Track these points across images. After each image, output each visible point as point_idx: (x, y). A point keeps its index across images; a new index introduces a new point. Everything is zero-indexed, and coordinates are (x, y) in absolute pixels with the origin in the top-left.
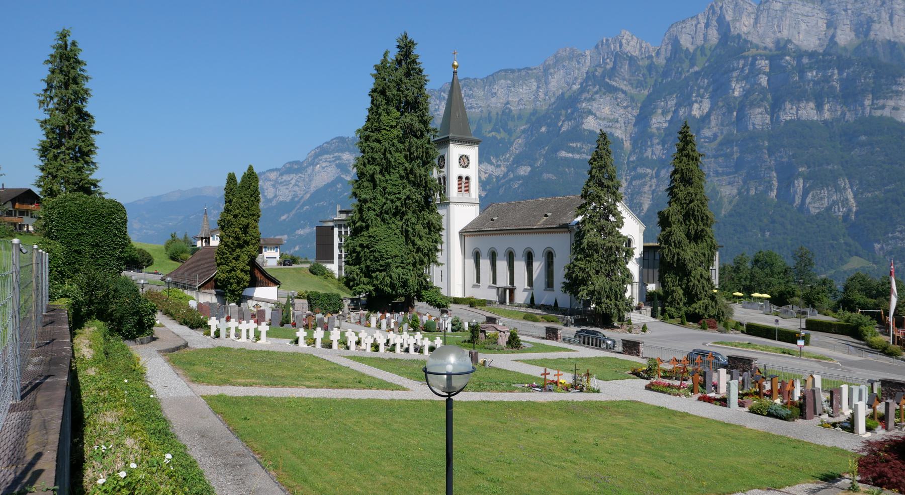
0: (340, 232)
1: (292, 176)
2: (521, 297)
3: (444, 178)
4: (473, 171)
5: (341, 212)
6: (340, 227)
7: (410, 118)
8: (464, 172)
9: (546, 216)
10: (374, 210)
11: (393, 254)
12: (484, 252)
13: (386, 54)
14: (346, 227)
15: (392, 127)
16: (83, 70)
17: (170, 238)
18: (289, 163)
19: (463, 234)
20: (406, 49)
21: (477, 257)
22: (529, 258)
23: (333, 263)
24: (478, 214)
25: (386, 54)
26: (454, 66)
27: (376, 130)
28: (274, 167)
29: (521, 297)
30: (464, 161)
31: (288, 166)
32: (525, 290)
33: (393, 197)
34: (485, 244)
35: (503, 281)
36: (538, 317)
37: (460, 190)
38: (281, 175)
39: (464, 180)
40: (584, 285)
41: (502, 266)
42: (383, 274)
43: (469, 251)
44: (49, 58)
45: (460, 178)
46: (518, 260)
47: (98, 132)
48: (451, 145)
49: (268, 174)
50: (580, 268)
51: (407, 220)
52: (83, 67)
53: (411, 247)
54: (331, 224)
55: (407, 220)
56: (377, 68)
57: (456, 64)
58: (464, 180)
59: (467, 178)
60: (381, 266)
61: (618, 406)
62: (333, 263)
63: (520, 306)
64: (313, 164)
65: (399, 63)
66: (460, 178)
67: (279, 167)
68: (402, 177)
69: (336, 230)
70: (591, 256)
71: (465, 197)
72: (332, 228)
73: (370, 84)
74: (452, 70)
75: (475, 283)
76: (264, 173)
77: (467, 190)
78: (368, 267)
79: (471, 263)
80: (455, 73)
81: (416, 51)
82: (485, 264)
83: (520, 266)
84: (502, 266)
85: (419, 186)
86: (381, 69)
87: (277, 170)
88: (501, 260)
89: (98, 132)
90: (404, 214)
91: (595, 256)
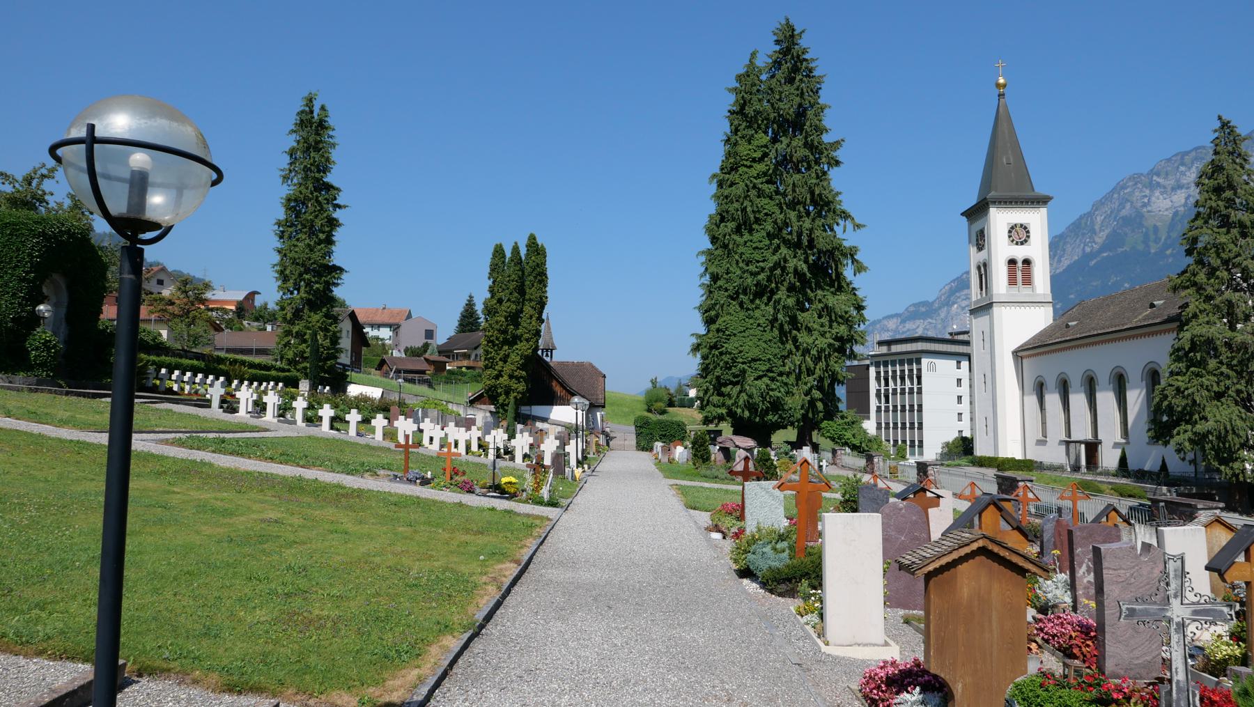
0: (878, 373)
1: (918, 322)
2: (1109, 458)
3: (985, 265)
4: (1037, 250)
5: (881, 343)
6: (877, 365)
7: (794, 145)
8: (1020, 253)
9: (1152, 306)
10: (726, 290)
11: (750, 355)
12: (1051, 382)
13: (753, 55)
14: (894, 364)
15: (754, 160)
16: (331, 137)
17: (650, 385)
18: (914, 305)
19: (1018, 354)
20: (788, 41)
21: (1040, 390)
22: (1120, 385)
23: (868, 418)
24: (1051, 321)
25: (753, 55)
26: (998, 85)
27: (732, 169)
28: (893, 313)
29: (1109, 458)
30: (1019, 234)
31: (912, 309)
32: (1116, 445)
33: (752, 268)
34: (1051, 366)
35: (1082, 432)
36: (1103, 487)
37: (1012, 281)
38: (903, 322)
39: (1020, 264)
40: (1187, 422)
41: (1078, 400)
42: (738, 388)
43: (1029, 384)
44: (293, 127)
45: (1012, 262)
46: (1101, 390)
47: (345, 207)
48: (993, 211)
49: (885, 322)
50: (1178, 389)
51: (778, 301)
52: (331, 133)
53: (790, 346)
54: (868, 362)
55: (778, 301)
56: (739, 78)
57: (1001, 81)
58: (1020, 264)
59: (1027, 262)
60: (735, 376)
61: (346, 496)
62: (868, 418)
63: (1106, 473)
64: (948, 303)
65: (777, 64)
66: (1012, 262)
67: (901, 311)
68: (770, 236)
69: (872, 370)
70: (1202, 363)
71: (1022, 292)
72: (868, 367)
73: (730, 100)
74: (996, 92)
75: (1040, 437)
76: (879, 321)
77: (1028, 280)
78: (718, 378)
79: (1032, 400)
80: (1001, 95)
81: (803, 42)
82: (1053, 400)
83: (1106, 399)
84: (1078, 400)
85: (797, 245)
86: (747, 79)
87: (897, 315)
88: (1076, 392)
89: (345, 207)
90: (773, 293)
91: (1212, 363)
